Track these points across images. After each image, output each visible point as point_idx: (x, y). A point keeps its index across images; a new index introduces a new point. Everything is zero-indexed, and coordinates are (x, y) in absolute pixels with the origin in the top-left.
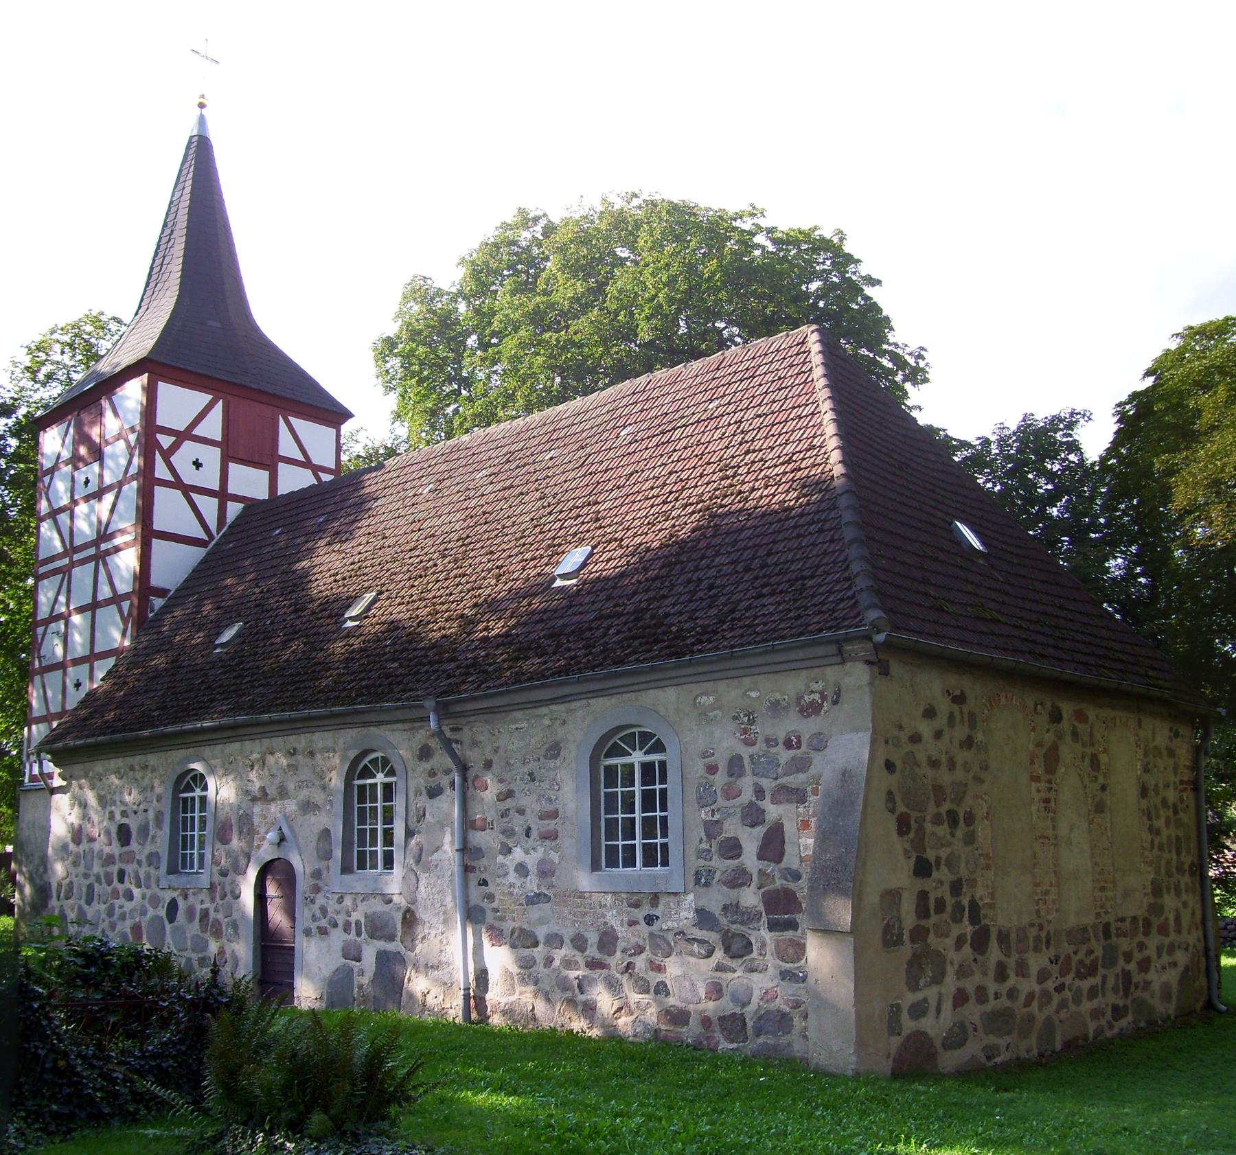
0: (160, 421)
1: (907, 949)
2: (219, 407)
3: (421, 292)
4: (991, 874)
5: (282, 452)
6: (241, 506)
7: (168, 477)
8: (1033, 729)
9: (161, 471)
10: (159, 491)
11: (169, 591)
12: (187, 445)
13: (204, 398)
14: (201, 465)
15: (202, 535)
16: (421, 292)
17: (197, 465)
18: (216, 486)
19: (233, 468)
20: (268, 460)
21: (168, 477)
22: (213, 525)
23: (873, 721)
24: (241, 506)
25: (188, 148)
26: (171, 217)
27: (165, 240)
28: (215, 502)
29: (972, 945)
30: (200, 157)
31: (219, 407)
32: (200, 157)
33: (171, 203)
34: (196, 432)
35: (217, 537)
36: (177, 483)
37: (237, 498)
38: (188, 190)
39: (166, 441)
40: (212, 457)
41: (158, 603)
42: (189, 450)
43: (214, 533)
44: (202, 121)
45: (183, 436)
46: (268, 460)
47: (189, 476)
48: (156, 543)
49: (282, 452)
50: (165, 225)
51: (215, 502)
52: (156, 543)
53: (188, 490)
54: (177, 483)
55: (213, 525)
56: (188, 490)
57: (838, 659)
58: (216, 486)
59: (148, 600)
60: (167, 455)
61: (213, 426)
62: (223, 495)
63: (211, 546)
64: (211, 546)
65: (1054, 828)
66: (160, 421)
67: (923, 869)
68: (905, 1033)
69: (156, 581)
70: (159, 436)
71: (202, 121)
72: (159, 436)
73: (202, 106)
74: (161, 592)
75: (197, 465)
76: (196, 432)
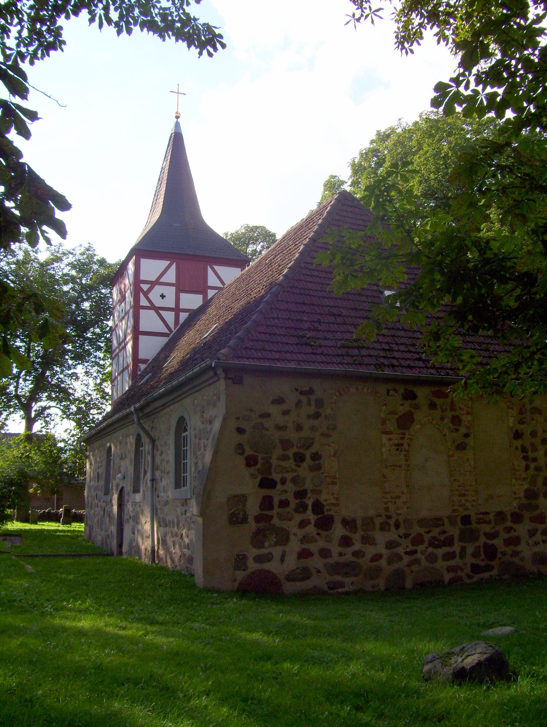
0: (142, 278)
1: (252, 525)
2: (174, 266)
3: (332, 184)
4: (337, 487)
5: (209, 284)
6: (188, 314)
7: (147, 304)
8: (385, 405)
9: (143, 302)
10: (142, 312)
11: (149, 360)
12: (157, 287)
13: (166, 263)
14: (165, 296)
15: (167, 331)
16: (332, 184)
17: (163, 296)
18: (173, 306)
19: (183, 296)
20: (201, 288)
21: (147, 304)
22: (172, 326)
23: (226, 408)
24: (188, 314)
25: (170, 140)
26: (162, 175)
27: (159, 187)
28: (172, 314)
29: (315, 526)
30: (177, 142)
31: (174, 266)
32: (177, 142)
33: (162, 168)
34: (161, 280)
35: (174, 331)
36: (152, 307)
37: (185, 311)
38: (169, 160)
39: (145, 287)
40: (171, 292)
41: (143, 367)
42: (158, 290)
43: (173, 330)
44: (177, 125)
45: (153, 284)
46: (201, 288)
47: (159, 302)
48: (141, 337)
49: (209, 284)
50: (159, 180)
51: (172, 314)
52: (141, 337)
53: (157, 309)
54: (152, 307)
55: (172, 326)
56: (157, 309)
57: (215, 378)
58: (173, 306)
59: (138, 366)
60: (146, 294)
61: (171, 276)
62: (177, 310)
63: (171, 336)
64: (171, 336)
65: (407, 460)
66: (142, 278)
67: (267, 483)
68: (249, 571)
69: (141, 356)
70: (141, 285)
71: (177, 125)
72: (141, 285)
73: (177, 117)
74: (145, 361)
75: (163, 296)
76: (161, 280)
